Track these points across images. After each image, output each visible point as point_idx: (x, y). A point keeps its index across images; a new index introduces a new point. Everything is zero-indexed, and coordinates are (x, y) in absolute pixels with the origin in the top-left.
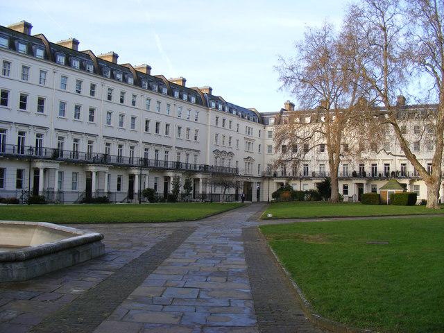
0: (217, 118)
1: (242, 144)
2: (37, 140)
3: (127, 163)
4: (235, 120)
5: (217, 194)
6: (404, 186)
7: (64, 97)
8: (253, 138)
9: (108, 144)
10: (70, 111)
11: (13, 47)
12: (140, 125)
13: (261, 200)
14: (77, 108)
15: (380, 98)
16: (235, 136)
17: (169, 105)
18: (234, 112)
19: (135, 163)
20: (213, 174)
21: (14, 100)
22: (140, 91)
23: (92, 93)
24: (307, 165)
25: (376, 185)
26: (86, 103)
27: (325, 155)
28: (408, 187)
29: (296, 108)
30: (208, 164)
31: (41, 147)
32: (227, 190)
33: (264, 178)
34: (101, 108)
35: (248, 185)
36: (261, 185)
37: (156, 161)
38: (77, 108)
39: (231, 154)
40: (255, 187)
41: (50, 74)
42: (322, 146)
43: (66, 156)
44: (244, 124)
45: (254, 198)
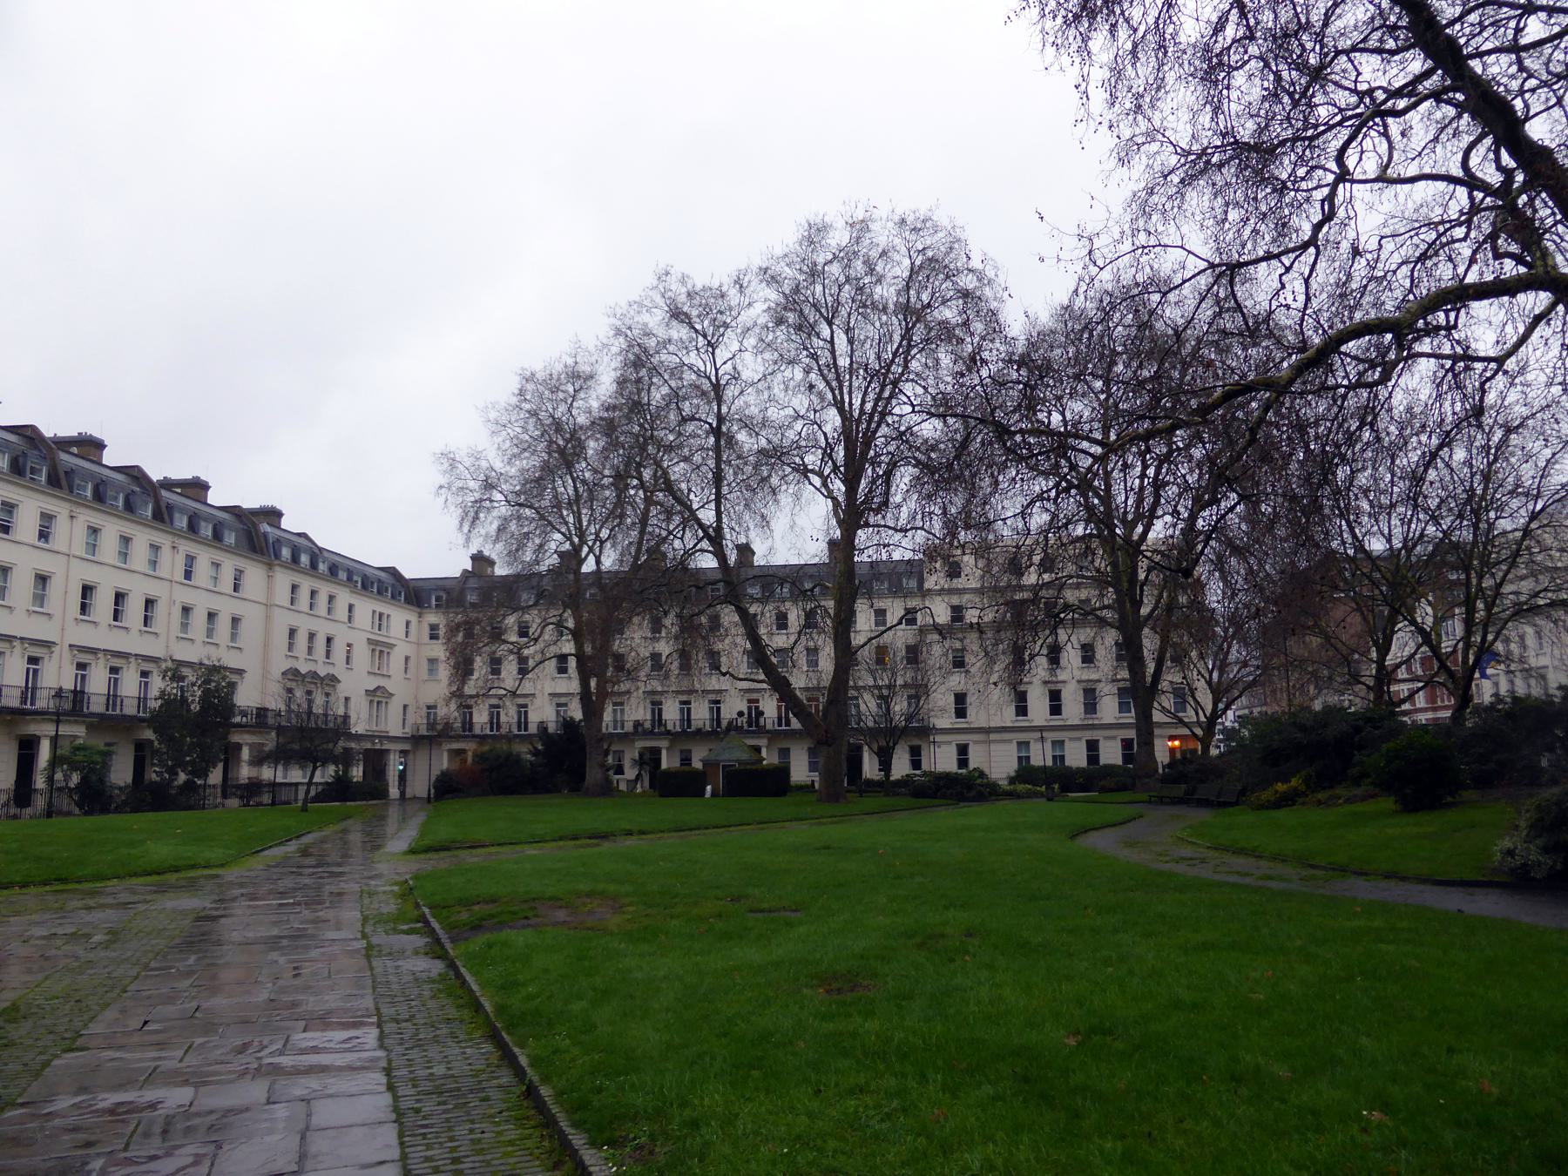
0: (294, 588)
1: (362, 654)
2: (28, 670)
3: (14, 702)
4: (344, 597)
5: (291, 784)
6: (758, 749)
7: (91, 574)
8: (391, 641)
9: (81, 666)
10: (103, 603)
11: (17, 469)
12: (64, 596)
13: (407, 796)
14: (119, 597)
15: (705, 544)
16: (342, 635)
17: (155, 548)
18: (343, 575)
19: (41, 704)
20: (280, 730)
21: (21, 587)
22: (67, 505)
23: (44, 535)
24: (525, 706)
25: (690, 751)
26: (227, 608)
27: (571, 684)
28: (764, 753)
29: (501, 570)
30: (268, 705)
31: (34, 689)
32: (318, 773)
33: (417, 740)
34: (170, 597)
35: (375, 762)
36: (411, 756)
37: (112, 698)
38: (119, 597)
39: (333, 680)
40: (395, 766)
41: (166, 553)
42: (562, 658)
43: (97, 706)
44: (366, 608)
45: (394, 792)
